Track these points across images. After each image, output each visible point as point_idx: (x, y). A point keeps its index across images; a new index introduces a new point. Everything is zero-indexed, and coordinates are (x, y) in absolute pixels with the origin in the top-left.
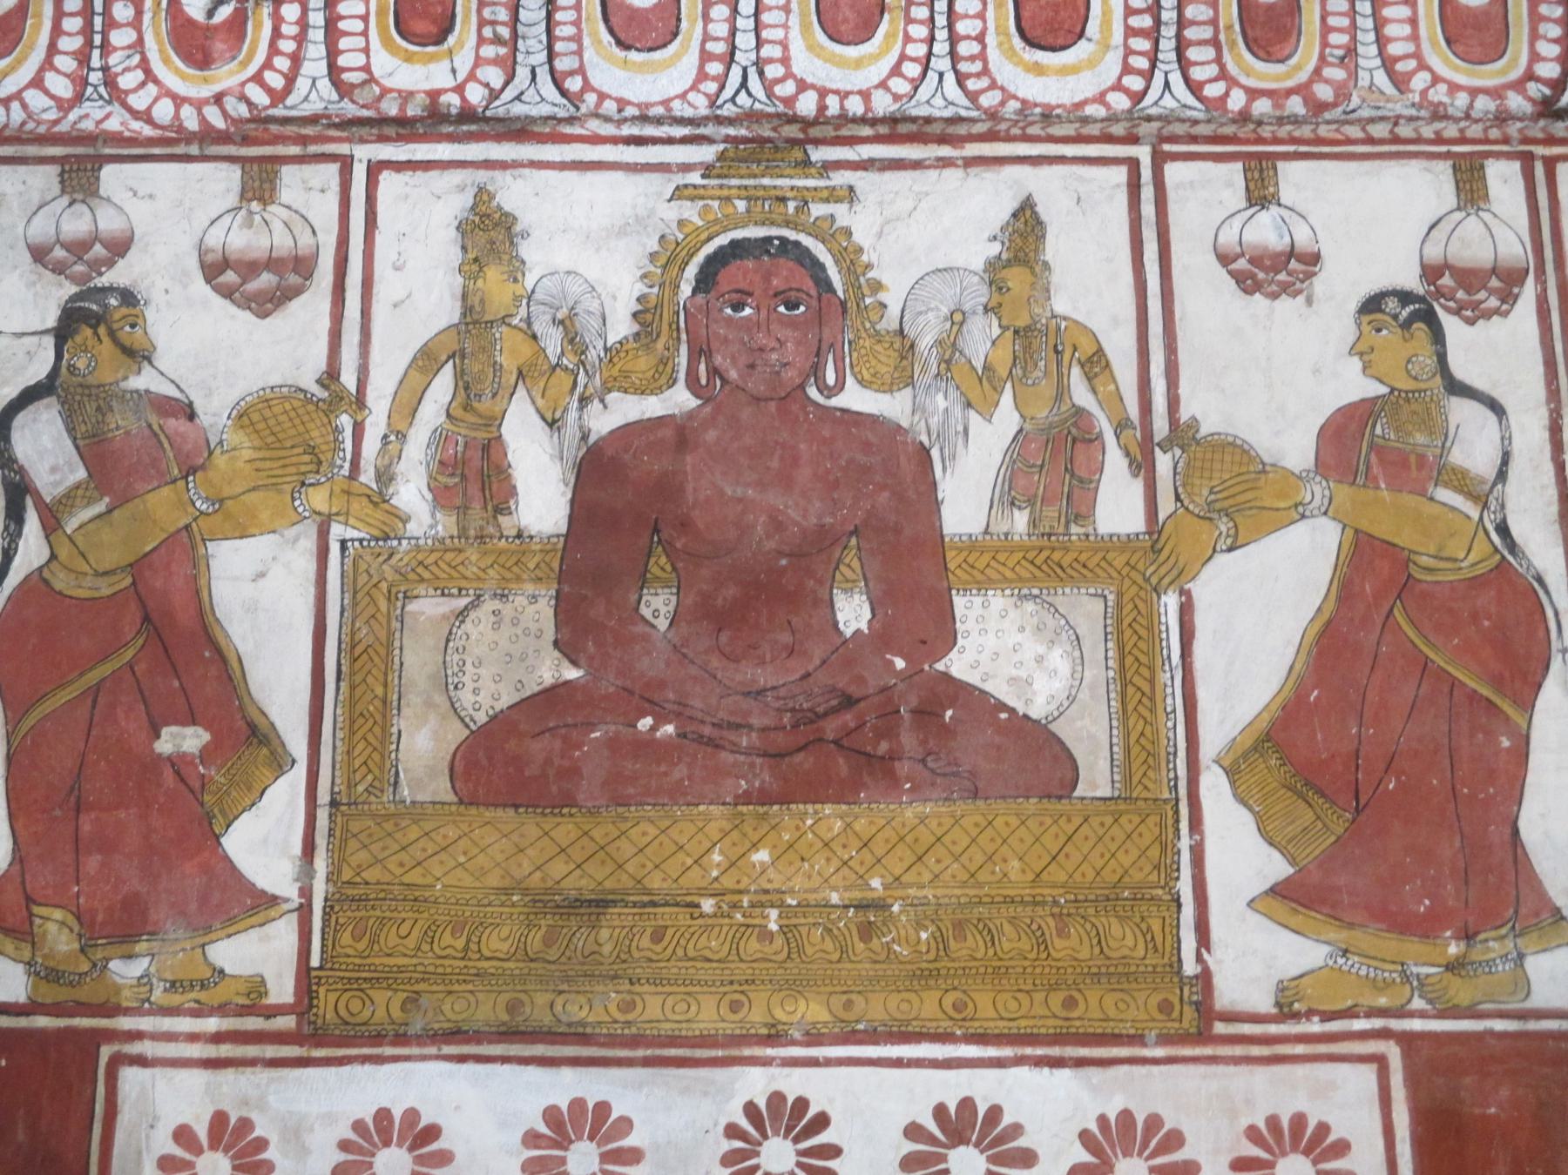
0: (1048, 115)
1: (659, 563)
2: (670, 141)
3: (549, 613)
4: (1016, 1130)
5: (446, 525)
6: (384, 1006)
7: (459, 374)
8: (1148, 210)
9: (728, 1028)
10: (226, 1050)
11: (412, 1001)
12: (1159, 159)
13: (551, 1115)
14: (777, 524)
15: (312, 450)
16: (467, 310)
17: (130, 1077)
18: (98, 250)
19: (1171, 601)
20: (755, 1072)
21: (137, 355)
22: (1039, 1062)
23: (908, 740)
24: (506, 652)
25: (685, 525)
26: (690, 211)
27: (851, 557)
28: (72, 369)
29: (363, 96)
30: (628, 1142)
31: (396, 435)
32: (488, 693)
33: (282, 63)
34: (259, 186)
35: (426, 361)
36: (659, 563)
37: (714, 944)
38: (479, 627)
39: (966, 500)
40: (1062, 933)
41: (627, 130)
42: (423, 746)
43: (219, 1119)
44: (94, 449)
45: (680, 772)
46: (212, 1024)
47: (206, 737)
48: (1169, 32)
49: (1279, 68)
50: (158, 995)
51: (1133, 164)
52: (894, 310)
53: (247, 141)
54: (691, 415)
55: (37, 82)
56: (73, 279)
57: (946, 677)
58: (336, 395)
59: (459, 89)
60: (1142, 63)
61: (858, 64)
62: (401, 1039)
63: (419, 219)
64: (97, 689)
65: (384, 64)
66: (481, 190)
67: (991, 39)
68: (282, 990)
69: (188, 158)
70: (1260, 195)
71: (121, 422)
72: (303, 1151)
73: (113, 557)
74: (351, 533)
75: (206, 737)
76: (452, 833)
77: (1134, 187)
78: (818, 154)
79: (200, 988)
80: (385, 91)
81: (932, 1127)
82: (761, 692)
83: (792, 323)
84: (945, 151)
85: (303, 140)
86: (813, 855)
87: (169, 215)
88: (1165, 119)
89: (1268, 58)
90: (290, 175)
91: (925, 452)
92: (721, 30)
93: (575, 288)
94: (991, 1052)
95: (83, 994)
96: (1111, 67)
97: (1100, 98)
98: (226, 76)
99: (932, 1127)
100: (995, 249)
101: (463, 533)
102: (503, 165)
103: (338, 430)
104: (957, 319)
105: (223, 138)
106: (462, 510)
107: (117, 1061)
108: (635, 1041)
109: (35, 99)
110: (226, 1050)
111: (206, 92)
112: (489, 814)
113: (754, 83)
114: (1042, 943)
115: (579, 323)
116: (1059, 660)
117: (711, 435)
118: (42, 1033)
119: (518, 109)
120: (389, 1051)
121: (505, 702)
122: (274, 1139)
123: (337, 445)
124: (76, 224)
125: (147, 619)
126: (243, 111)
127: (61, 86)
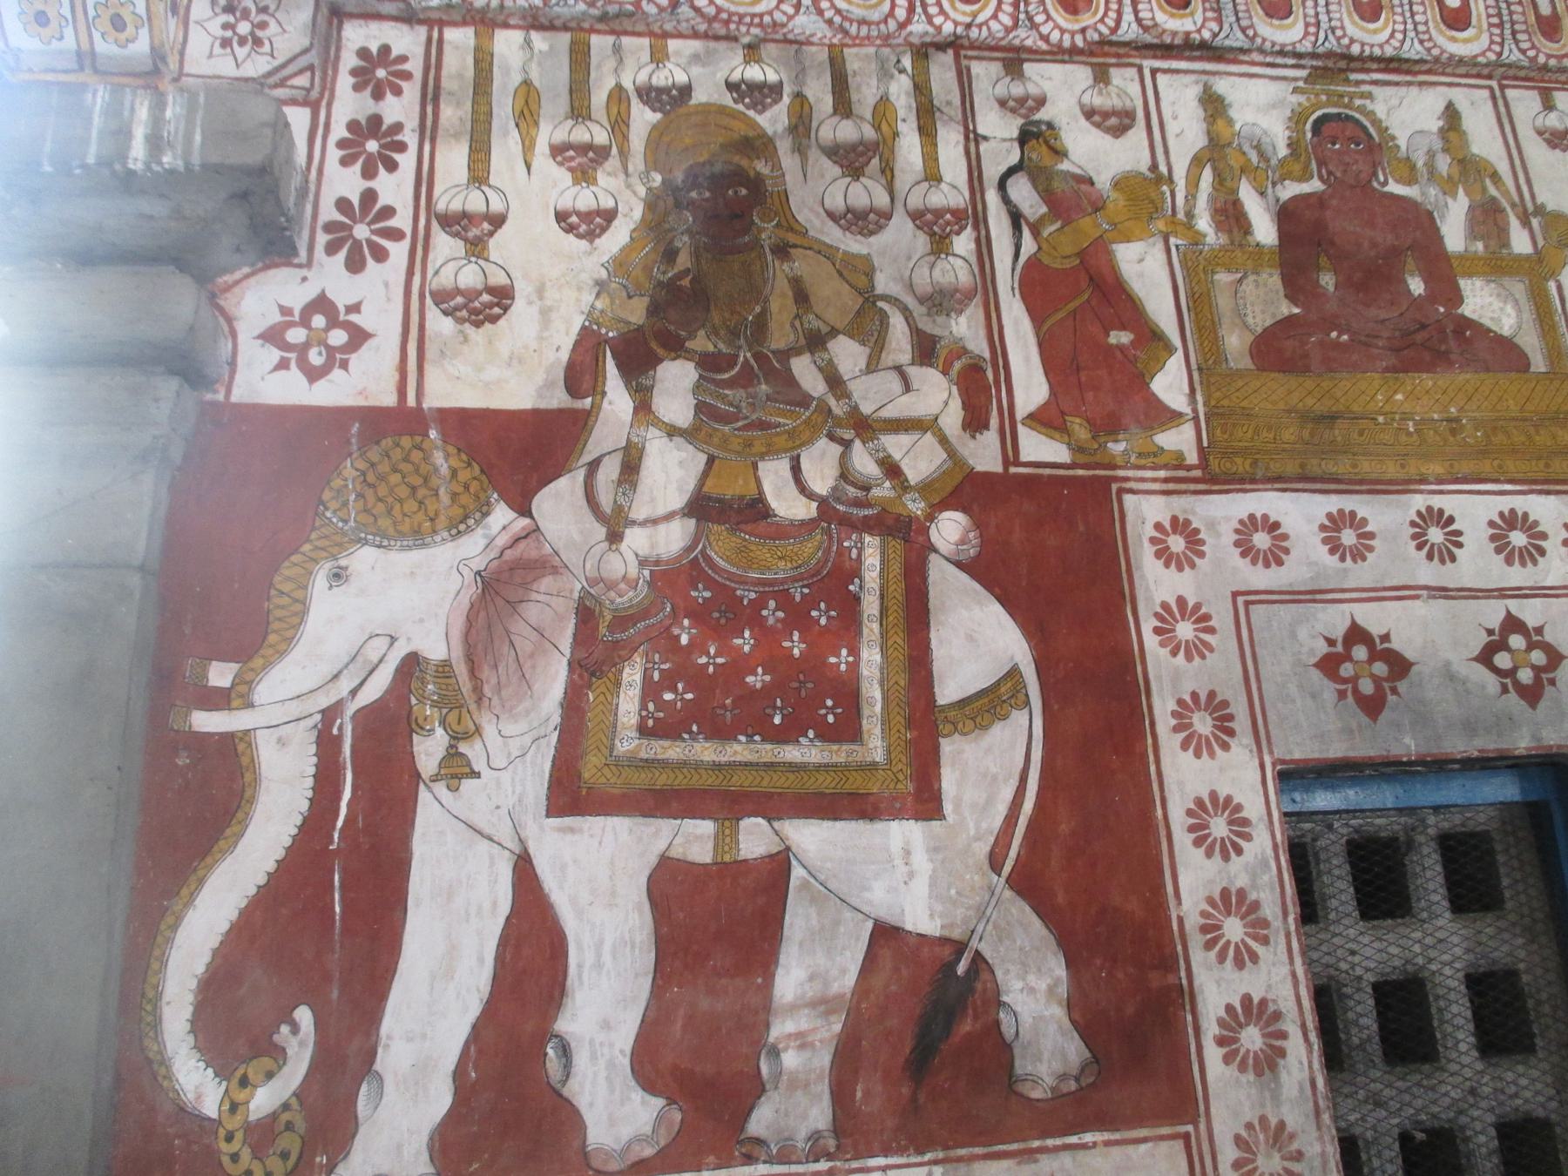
0: (1461, 61)
1: (1323, 261)
2: (1285, 66)
3: (1279, 282)
4: (1536, 523)
5: (1223, 239)
6: (1241, 465)
7: (1214, 169)
8: (1502, 109)
9: (1401, 476)
10: (1171, 486)
11: (1255, 463)
12: (1502, 88)
13: (1329, 516)
14: (1374, 245)
15: (1152, 202)
16: (1211, 140)
17: (1128, 499)
18: (1030, 103)
19: (1552, 285)
20: (1418, 497)
21: (1060, 153)
22: (1540, 492)
23: (1452, 344)
24: (1261, 301)
25: (1332, 243)
26: (1302, 99)
27: (1410, 260)
28: (1030, 159)
29: (1154, 32)
30: (1196, 560)
31: (1191, 197)
32: (1260, 320)
33: (1113, 15)
34: (1101, 77)
35: (1197, 162)
36: (1323, 261)
37: (1387, 437)
38: (1248, 287)
39: (1454, 234)
40: (1537, 433)
41: (1268, 59)
42: (1235, 343)
43: (1174, 519)
44: (1048, 196)
45: (1355, 357)
46: (1162, 474)
47: (1132, 337)
48: (1507, 26)
49: (1556, 46)
50: (1133, 459)
51: (1491, 88)
52: (1403, 148)
53: (1092, 54)
54: (1323, 192)
55: (995, 17)
56: (1021, 116)
57: (1463, 316)
58: (1158, 178)
59: (1199, 31)
60: (1498, 39)
61: (1375, 32)
62: (1253, 481)
63: (1179, 97)
64: (1075, 311)
65: (1161, 17)
66: (1205, 85)
67: (1431, 24)
68: (1192, 458)
69: (1064, 62)
70: (1548, 106)
71: (1058, 185)
72: (1218, 535)
73: (1069, 250)
74: (1180, 242)
75: (1132, 337)
76: (1258, 384)
77: (1494, 98)
78: (1353, 77)
79: (1154, 457)
80: (1164, 31)
81: (1499, 521)
82: (1383, 321)
83: (1357, 152)
84: (1409, 78)
85: (1118, 56)
86: (1421, 397)
87: (1062, 89)
88: (1510, 66)
89: (1551, 40)
90: (1113, 71)
91: (1430, 214)
92: (1311, 12)
93: (1258, 132)
94: (1518, 488)
95: (1098, 458)
96: (1484, 41)
97: (1483, 54)
98: (1087, 19)
99: (1499, 521)
100: (1441, 123)
101: (1232, 243)
102: (1214, 73)
103: (1163, 193)
104: (1431, 154)
105: (1081, 52)
106: (1230, 232)
107: (1121, 491)
108: (1361, 482)
109: (994, 25)
110: (1171, 486)
111: (1077, 27)
112: (1273, 375)
113: (1331, 37)
114: (1530, 437)
115: (1264, 147)
116: (1509, 309)
117: (1334, 202)
118: (1081, 477)
119: (1227, 43)
120: (1248, 487)
121: (1268, 323)
122: (1202, 529)
123: (1163, 201)
124: (1017, 90)
125: (1091, 279)
126: (1096, 37)
127: (1007, 20)
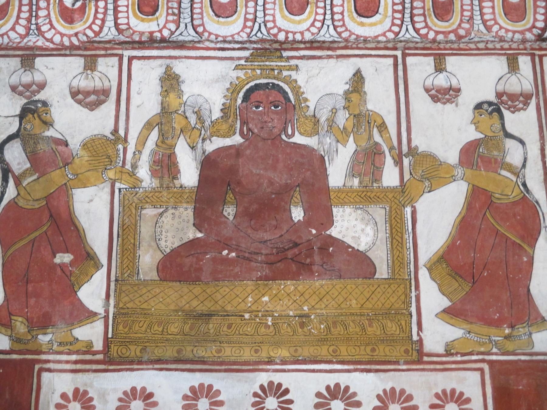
0: (366, 40)
1: (230, 197)
2: (234, 49)
3: (192, 214)
4: (355, 394)
5: (155, 183)
6: (134, 351)
7: (160, 131)
8: (401, 73)
9: (254, 359)
10: (79, 366)
11: (144, 349)
12: (404, 56)
13: (192, 389)
14: (271, 183)
15: (109, 157)
16: (163, 108)
17: (45, 376)
18: (34, 87)
19: (408, 210)
20: (264, 374)
21: (48, 124)
22: (362, 371)
23: (317, 258)
24: (176, 227)
25: (239, 183)
26: (241, 74)
27: (297, 194)
28: (25, 129)
29: (127, 33)
30: (219, 398)
31: (138, 152)
32: (170, 242)
33: (98, 22)
34: (90, 65)
35: (149, 126)
36: (230, 197)
37: (249, 329)
38: (167, 219)
39: (337, 175)
40: (370, 325)
41: (219, 45)
42: (148, 260)
43: (76, 390)
44: (33, 157)
45: (237, 269)
46: (74, 357)
47: (72, 257)
48: (408, 11)
49: (446, 24)
50: (55, 347)
51: (395, 57)
52: (312, 108)
53: (86, 49)
54: (241, 145)
55: (13, 29)
56: (26, 97)
57: (330, 236)
58: (117, 138)
59: (160, 31)
60: (398, 22)
61: (299, 22)
62: (140, 363)
63: (146, 77)
64: (34, 240)
65: (134, 22)
66: (168, 66)
67: (346, 14)
68: (98, 345)
69: (65, 55)
70: (440, 68)
71: (42, 147)
72: (106, 402)
73: (39, 194)
74: (122, 186)
75: (72, 257)
76: (158, 291)
77: (396, 65)
78: (285, 54)
79: (70, 345)
80: (134, 32)
81: (325, 393)
82: (266, 241)
83: (276, 113)
84: (330, 53)
85: (106, 49)
86: (284, 298)
87: (59, 75)
88: (406, 42)
89: (442, 20)
90: (101, 61)
91: (323, 158)
92: (251, 10)
93: (200, 101)
94: (346, 367)
95: (29, 347)
96: (388, 23)
97: (384, 34)
98: (79, 27)
99: (325, 393)
100: (347, 87)
101: (161, 186)
102: (176, 58)
103: (118, 150)
104: (334, 111)
105: (78, 48)
106: (161, 178)
107: (41, 370)
108: (221, 363)
109: (12, 34)
110: (79, 366)
111: (72, 32)
112: (171, 284)
113: (263, 29)
114: (364, 329)
115: (202, 113)
116: (369, 230)
117: (248, 152)
118: (15, 360)
119: (181, 38)
120: (136, 367)
121: (176, 245)
122: (95, 397)
123: (118, 155)
124: (27, 78)
125: (51, 216)
126: (85, 39)
127: (21, 30)
